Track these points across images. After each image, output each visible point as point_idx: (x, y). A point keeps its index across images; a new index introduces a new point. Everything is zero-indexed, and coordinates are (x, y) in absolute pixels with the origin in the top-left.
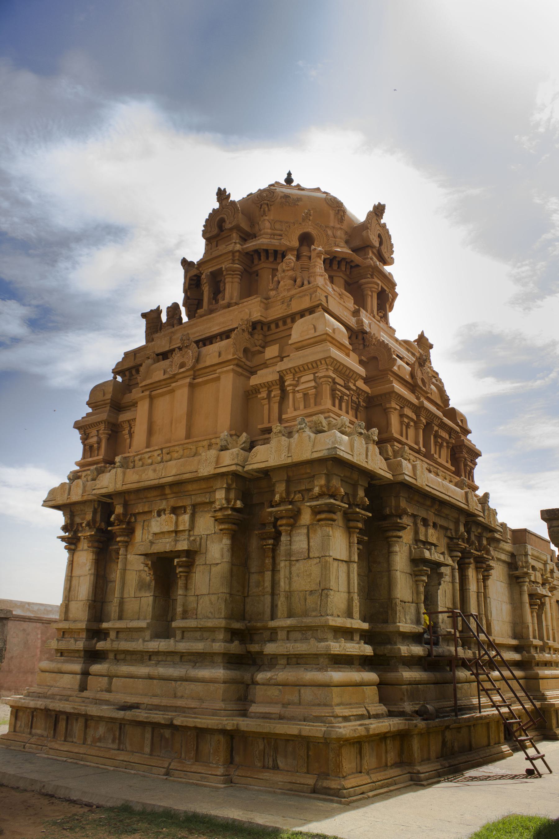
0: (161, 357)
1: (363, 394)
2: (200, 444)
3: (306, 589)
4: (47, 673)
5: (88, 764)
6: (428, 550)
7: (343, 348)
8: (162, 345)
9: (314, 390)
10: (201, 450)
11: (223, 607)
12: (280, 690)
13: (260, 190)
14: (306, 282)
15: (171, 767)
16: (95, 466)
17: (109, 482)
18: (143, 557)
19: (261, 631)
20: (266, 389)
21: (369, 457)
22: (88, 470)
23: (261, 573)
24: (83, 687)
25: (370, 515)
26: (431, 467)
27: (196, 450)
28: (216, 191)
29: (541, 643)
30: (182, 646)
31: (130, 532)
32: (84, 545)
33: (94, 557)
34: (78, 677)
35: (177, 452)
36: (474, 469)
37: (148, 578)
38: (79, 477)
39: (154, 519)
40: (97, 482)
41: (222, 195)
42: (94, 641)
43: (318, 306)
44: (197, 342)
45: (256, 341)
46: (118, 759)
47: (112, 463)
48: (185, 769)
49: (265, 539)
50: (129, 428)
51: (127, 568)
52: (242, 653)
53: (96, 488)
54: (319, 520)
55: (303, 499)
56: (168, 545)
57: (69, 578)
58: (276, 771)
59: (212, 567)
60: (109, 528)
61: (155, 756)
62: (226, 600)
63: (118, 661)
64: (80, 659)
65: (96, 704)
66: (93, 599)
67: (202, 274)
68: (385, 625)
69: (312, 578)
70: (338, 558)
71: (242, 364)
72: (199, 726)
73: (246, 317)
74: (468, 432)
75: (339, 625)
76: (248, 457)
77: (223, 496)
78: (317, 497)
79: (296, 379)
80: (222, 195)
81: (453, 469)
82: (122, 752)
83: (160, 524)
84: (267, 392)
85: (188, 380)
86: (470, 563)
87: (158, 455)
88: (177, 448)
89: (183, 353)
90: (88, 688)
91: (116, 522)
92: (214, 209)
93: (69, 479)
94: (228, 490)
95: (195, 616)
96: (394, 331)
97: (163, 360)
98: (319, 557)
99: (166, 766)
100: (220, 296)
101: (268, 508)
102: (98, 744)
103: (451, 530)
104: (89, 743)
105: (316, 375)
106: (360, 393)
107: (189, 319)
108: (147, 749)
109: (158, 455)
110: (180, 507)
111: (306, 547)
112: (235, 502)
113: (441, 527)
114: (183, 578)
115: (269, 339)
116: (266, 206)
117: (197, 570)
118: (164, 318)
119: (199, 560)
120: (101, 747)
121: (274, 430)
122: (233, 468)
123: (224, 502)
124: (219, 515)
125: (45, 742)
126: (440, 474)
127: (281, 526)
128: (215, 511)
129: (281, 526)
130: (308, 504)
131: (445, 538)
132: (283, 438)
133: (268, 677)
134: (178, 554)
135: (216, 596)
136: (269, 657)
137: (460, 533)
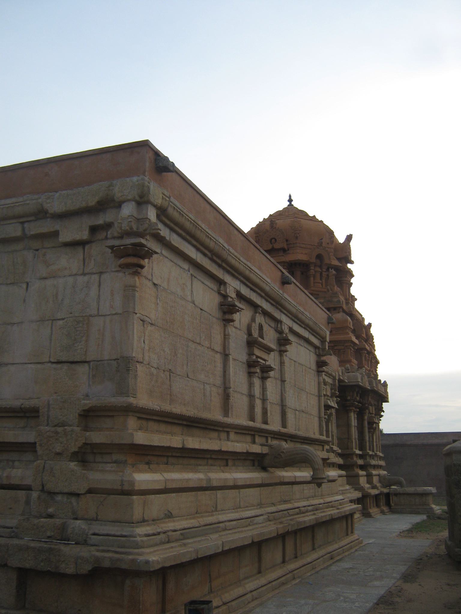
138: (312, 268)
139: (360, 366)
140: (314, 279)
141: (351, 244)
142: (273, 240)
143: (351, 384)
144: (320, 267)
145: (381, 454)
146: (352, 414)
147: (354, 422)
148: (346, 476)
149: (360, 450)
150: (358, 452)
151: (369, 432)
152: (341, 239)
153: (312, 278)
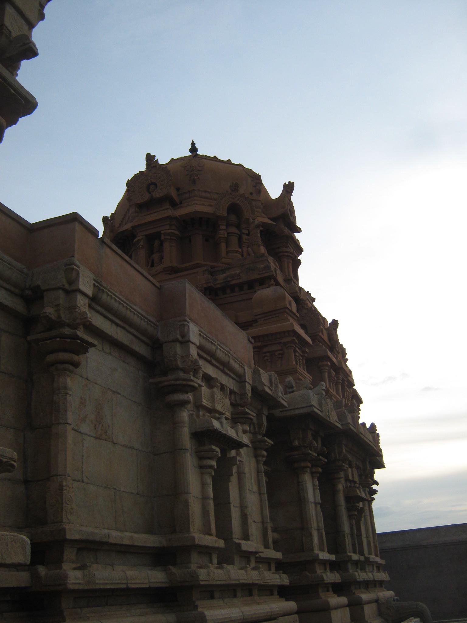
29: (221, 543)
80: (150, 159)
138: (222, 227)
139: (315, 383)
140: (227, 247)
141: (293, 199)
142: (152, 187)
143: (297, 412)
144: (238, 227)
145: (378, 559)
146: (307, 478)
147: (311, 491)
148: (349, 605)
149: (330, 552)
150: (324, 555)
151: (350, 517)
152: (275, 192)
153: (223, 245)
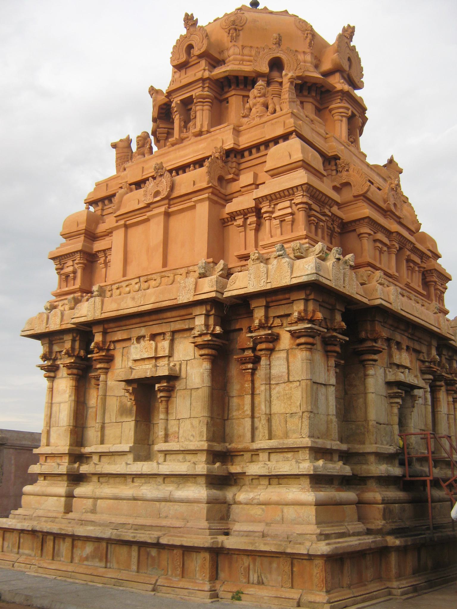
0: (133, 186)
1: (338, 220)
2: (178, 271)
3: (287, 412)
4: (32, 497)
5: (77, 581)
6: (402, 373)
7: (318, 174)
8: (134, 174)
9: (291, 217)
10: (178, 278)
11: (205, 430)
12: (263, 510)
13: (226, 15)
14: (278, 109)
15: (158, 584)
16: (72, 296)
17: (87, 311)
18: (124, 383)
19: (242, 453)
20: (242, 216)
21: (347, 282)
22: (65, 299)
23: (241, 396)
24: (68, 509)
25: (348, 339)
26: (404, 292)
27: (174, 277)
28: (184, 16)
30: (166, 468)
31: (109, 359)
32: (63, 372)
33: (74, 384)
34: (63, 499)
35: (155, 280)
36: (444, 293)
37: (129, 404)
38: (55, 307)
39: (133, 346)
40: (75, 311)
41: (190, 21)
42: (76, 465)
43: (290, 133)
44: (170, 171)
45: (230, 169)
46: (106, 576)
47: (89, 292)
48: (172, 585)
49: (244, 363)
50: (104, 258)
51: (107, 394)
52: (224, 474)
53: (74, 317)
54: (299, 345)
55: (282, 325)
56: (149, 371)
57: (50, 404)
58: (261, 586)
59: (193, 391)
60: (89, 356)
61: (142, 573)
62: (207, 422)
63: (102, 484)
64: (63, 482)
65: (82, 524)
66: (75, 425)
67: (172, 102)
68: (361, 446)
69: (292, 401)
70: (318, 381)
71: (217, 192)
72: (185, 544)
73: (219, 145)
74: (438, 256)
75: (320, 446)
76: (227, 284)
77: (203, 323)
78: (296, 322)
79: (273, 206)
80: (190, 21)
81: (425, 293)
82: (110, 570)
83: (139, 350)
84: (243, 220)
85: (162, 209)
86: (441, 386)
87: (136, 283)
88: (154, 276)
89: (157, 183)
90: (73, 510)
91: (96, 349)
92: (181, 35)
93: (46, 309)
94: (207, 316)
95: (177, 440)
96: (365, 156)
97: (137, 189)
98: (298, 381)
99: (154, 582)
100: (191, 124)
101: (247, 333)
102: (86, 563)
103: (423, 353)
104: (76, 561)
105: (293, 202)
106: (335, 218)
107: (158, 149)
108: (134, 567)
109: (136, 283)
110: (160, 334)
111: (286, 370)
112: (214, 328)
113: (415, 350)
114: (164, 403)
115: (243, 166)
116: (234, 31)
117: (178, 394)
118: (134, 147)
119: (179, 385)
120: (89, 565)
121: (252, 257)
122: (213, 295)
123: (204, 328)
124: (199, 340)
125: (33, 561)
126: (413, 298)
127: (261, 350)
128: (194, 337)
129: (261, 350)
130: (288, 329)
131: (418, 361)
132: (262, 264)
133: (251, 497)
134: (159, 379)
135: (197, 420)
136: (251, 478)
137: (432, 357)
